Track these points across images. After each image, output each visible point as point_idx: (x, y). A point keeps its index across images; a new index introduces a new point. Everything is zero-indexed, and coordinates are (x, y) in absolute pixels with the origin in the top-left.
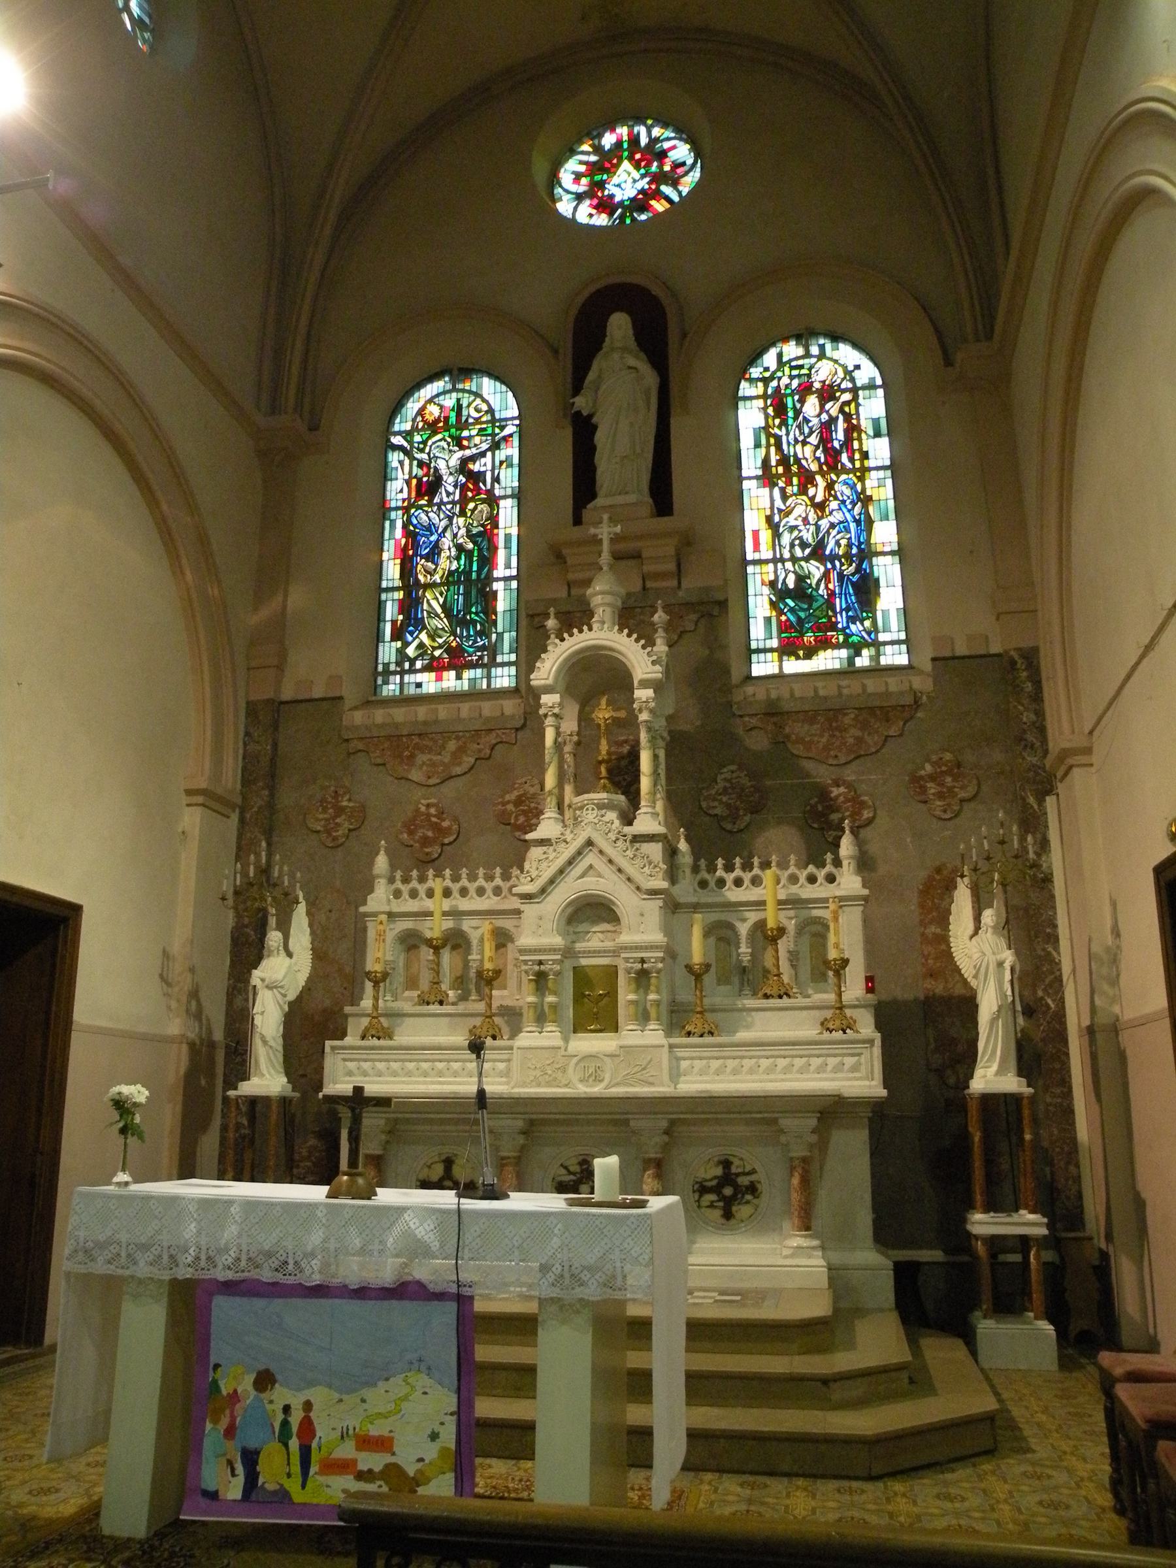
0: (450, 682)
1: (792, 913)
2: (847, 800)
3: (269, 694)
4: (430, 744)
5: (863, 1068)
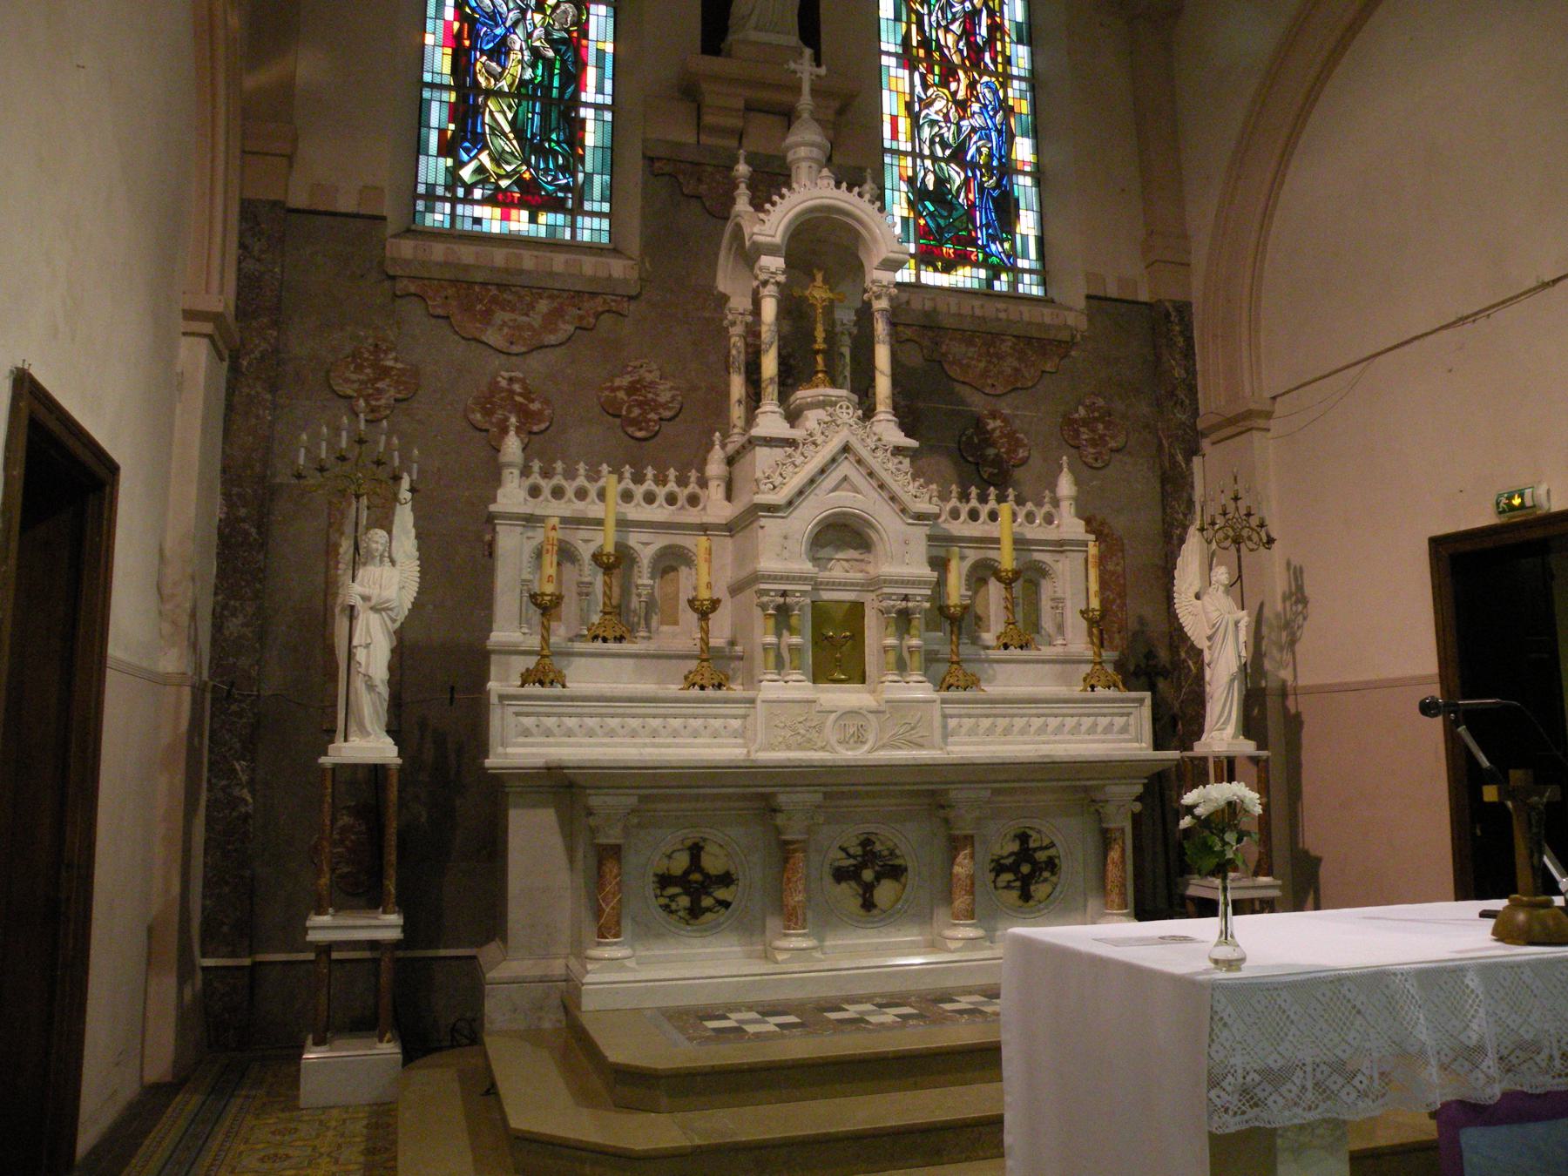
0: (520, 222)
2: (1003, 435)
5: (1132, 729)
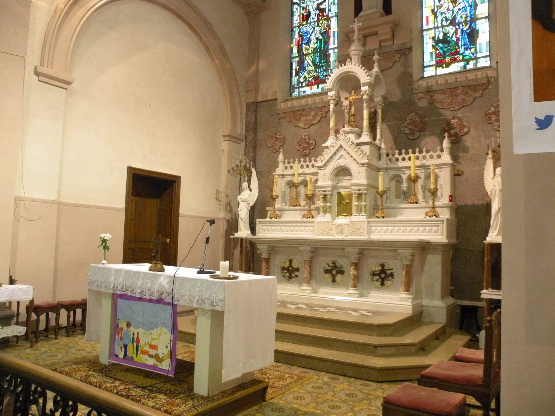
1: (423, 171)
3: (253, 100)
4: (305, 113)
5: (439, 231)
